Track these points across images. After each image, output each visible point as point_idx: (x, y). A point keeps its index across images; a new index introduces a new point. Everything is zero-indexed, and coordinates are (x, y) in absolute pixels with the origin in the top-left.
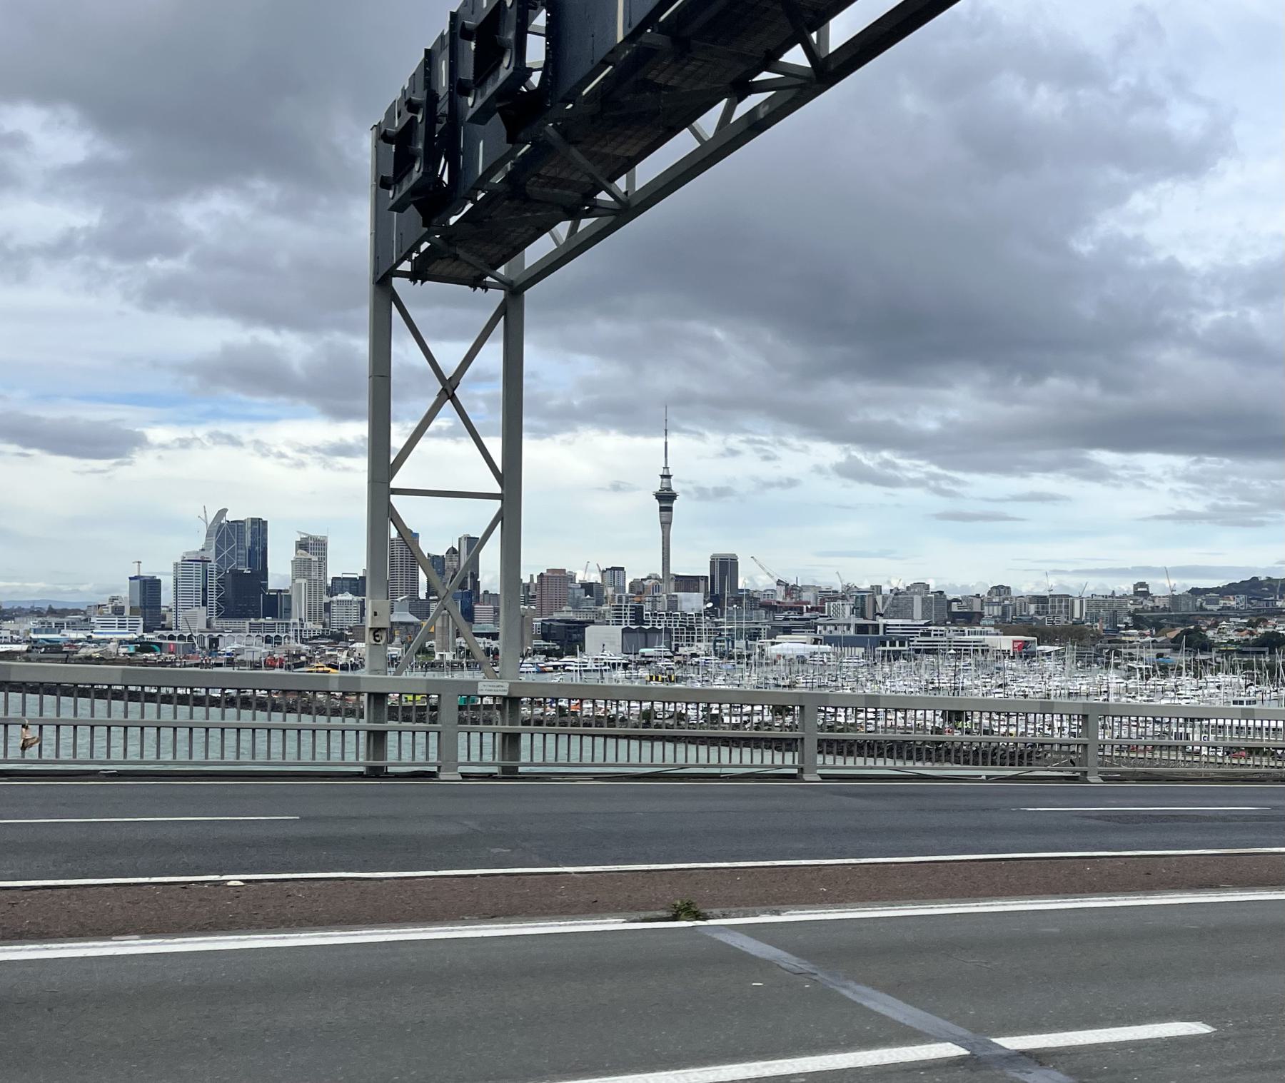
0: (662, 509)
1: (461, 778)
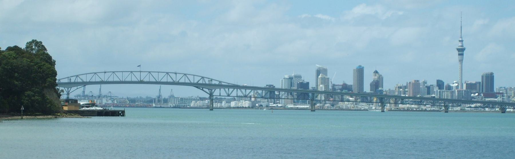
0: (459, 55)
1: (226, 95)
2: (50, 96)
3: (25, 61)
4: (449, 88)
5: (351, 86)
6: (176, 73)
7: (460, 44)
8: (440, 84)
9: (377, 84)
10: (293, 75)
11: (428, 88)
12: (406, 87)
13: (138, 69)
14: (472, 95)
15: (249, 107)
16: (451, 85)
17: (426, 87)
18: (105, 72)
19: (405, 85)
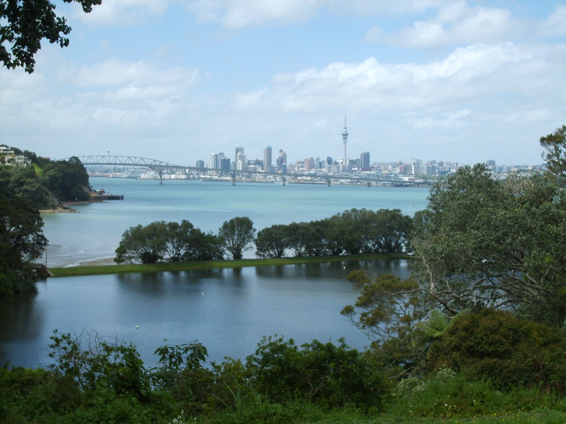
0: (344, 138)
2: (86, 190)
3: (72, 170)
4: (336, 163)
5: (262, 161)
6: (135, 157)
7: (345, 130)
8: (330, 161)
9: (281, 161)
10: (218, 153)
11: (320, 163)
12: (303, 163)
13: (108, 154)
14: (353, 169)
15: (185, 179)
16: (338, 161)
17: (319, 162)
18: (84, 157)
19: (303, 160)
